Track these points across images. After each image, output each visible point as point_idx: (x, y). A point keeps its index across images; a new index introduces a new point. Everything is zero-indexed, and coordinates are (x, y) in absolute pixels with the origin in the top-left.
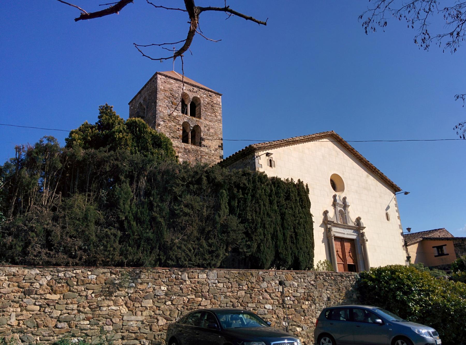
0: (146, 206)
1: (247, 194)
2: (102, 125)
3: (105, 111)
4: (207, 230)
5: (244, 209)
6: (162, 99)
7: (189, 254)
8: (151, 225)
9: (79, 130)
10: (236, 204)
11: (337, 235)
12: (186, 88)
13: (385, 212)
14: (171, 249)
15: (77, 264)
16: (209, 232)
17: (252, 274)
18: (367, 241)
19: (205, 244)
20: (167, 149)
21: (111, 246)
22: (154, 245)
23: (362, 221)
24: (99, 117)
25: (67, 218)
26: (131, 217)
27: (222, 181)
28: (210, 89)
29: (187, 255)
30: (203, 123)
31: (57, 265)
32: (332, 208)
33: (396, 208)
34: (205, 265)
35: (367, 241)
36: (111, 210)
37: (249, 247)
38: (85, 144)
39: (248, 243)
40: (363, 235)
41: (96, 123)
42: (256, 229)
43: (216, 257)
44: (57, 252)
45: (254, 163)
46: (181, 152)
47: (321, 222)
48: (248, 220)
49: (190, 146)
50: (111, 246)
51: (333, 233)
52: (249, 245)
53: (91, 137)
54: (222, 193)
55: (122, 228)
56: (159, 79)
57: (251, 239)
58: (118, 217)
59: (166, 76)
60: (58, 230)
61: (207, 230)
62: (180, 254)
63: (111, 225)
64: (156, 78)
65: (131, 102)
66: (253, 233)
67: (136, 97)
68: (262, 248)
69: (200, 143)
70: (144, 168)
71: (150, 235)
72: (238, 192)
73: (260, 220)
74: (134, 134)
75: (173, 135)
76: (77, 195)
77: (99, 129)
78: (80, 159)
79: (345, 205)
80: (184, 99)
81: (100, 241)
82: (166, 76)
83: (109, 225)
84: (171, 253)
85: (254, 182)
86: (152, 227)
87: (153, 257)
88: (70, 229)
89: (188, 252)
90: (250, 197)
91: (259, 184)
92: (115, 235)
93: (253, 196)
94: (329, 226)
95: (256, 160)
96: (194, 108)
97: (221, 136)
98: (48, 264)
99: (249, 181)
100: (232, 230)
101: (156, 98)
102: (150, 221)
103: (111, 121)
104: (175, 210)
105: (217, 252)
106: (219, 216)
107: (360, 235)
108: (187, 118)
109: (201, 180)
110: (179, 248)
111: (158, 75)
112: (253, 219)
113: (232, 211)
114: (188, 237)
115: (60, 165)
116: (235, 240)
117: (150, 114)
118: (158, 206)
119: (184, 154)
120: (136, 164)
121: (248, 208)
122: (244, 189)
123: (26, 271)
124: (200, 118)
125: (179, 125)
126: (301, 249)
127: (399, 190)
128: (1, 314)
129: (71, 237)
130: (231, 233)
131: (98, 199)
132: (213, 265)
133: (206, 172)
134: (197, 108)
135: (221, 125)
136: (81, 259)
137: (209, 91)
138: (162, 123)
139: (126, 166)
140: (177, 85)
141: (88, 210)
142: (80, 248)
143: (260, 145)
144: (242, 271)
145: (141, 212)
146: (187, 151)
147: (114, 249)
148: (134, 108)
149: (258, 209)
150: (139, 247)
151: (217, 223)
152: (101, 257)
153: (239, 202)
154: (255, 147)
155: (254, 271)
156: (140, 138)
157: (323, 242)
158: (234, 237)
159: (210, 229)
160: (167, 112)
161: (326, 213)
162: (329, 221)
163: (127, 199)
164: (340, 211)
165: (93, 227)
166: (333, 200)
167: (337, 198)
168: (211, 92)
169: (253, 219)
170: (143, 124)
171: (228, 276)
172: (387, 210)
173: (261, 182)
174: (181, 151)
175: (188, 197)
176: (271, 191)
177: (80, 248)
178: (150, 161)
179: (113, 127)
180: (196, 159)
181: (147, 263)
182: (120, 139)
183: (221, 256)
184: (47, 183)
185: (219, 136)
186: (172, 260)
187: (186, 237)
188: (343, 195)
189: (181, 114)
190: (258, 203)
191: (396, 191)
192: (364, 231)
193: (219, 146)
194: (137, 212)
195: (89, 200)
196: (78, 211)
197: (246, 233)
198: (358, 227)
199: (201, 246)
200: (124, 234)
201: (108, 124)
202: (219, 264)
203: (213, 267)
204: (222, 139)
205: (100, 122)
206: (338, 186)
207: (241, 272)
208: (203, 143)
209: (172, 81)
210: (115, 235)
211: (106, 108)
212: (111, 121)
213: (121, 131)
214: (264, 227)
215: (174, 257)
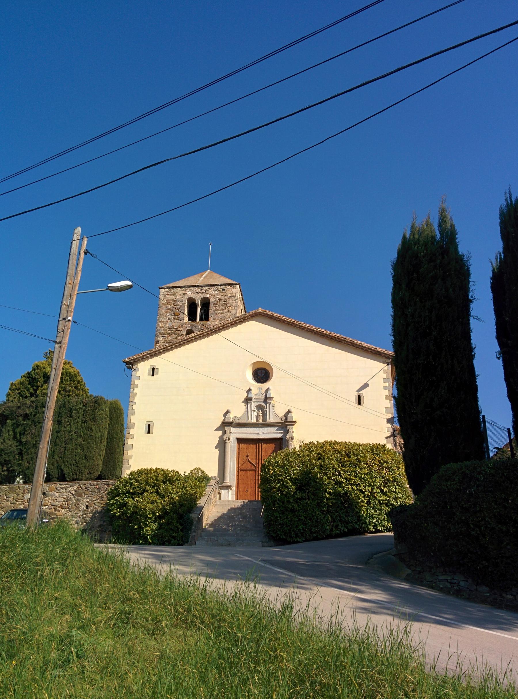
6: (163, 314)
12: (190, 293)
13: (356, 394)
59: (169, 288)
82: (169, 288)
128: (251, 698)
140: (181, 293)
203: (149, 503)
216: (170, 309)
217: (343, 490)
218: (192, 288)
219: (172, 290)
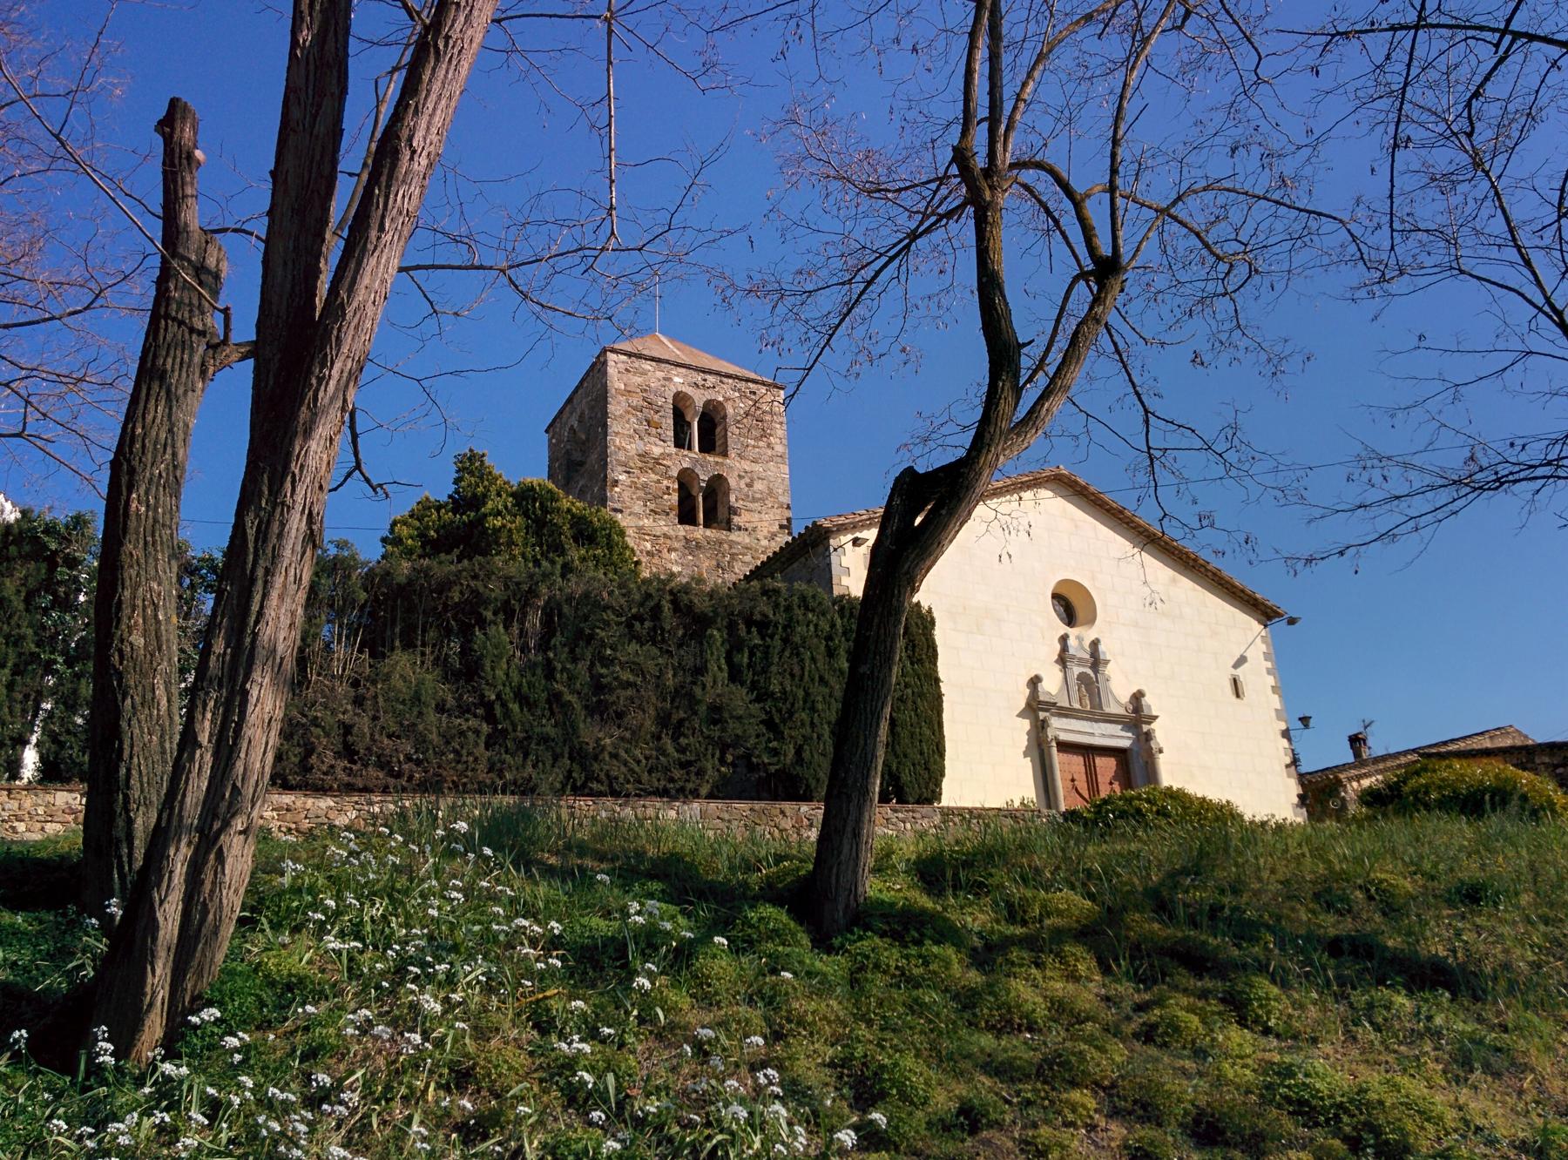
0: (539, 671)
1: (772, 637)
2: (463, 498)
3: (470, 465)
4: (675, 718)
5: (765, 671)
6: (621, 416)
7: (637, 769)
8: (551, 709)
9: (411, 516)
10: (746, 660)
11: (1063, 737)
12: (679, 380)
14: (596, 758)
15: (404, 790)
16: (681, 722)
17: (782, 812)
18: (1161, 751)
19: (670, 749)
20: (610, 546)
21: (469, 754)
22: (558, 750)
23: (1147, 700)
24: (457, 481)
25: (380, 699)
26: (508, 694)
27: (709, 611)
28: (753, 376)
29: (632, 771)
30: (734, 468)
31: (366, 790)
32: (1058, 667)
33: (1269, 665)
34: (673, 792)
35: (1161, 751)
36: (468, 682)
37: (775, 752)
38: (423, 546)
39: (774, 744)
40: (1148, 736)
41: (450, 497)
42: (791, 714)
43: (697, 774)
44: (366, 766)
45: (829, 565)
46: (675, 550)
47: (1022, 705)
48: (773, 693)
49: (699, 532)
50: (469, 754)
51: (1050, 733)
52: (775, 749)
53: (437, 531)
54: (712, 636)
55: (490, 718)
56: (611, 363)
57: (779, 736)
58: (482, 696)
59: (630, 355)
60: (364, 724)
61: (675, 718)
62: (618, 770)
63: (468, 711)
64: (605, 363)
65: (551, 425)
66: (784, 721)
67: (561, 412)
68: (806, 755)
69: (729, 521)
70: (533, 592)
71: (550, 730)
72: (749, 632)
73: (801, 693)
74: (528, 517)
75: (653, 506)
76: (398, 652)
77: (455, 512)
78: (402, 580)
79: (1096, 661)
80: (680, 405)
81: (448, 743)
82: (630, 355)
83: (464, 710)
84: (596, 766)
85: (788, 609)
86: (552, 714)
87: (556, 777)
88: (387, 720)
89: (634, 766)
90: (777, 642)
91: (798, 612)
92: (477, 732)
93: (785, 641)
94: (1042, 715)
95: (834, 557)
96: (710, 430)
97: (785, 499)
98: (349, 789)
99: (777, 606)
100: (732, 717)
101: (605, 414)
102: (548, 701)
103: (480, 489)
104: (602, 676)
105: (698, 765)
106: (704, 687)
107: (1143, 738)
108: (689, 458)
109: (676, 615)
110: (615, 756)
111: (611, 356)
112: (784, 692)
113: (735, 676)
114: (633, 733)
115: (363, 596)
116: (738, 741)
117: (594, 457)
118: (564, 669)
119: (684, 555)
120: (518, 584)
121: (774, 669)
122: (763, 626)
123: (310, 801)
124: (725, 454)
125: (669, 478)
126: (905, 756)
127: (1279, 615)
129: (389, 737)
130: (731, 724)
131: (441, 661)
132: (691, 792)
133: (671, 592)
134: (718, 430)
135: (786, 469)
136: (410, 778)
137: (748, 380)
138: (623, 477)
139: (495, 589)
140: (660, 374)
141: (421, 683)
142: (409, 758)
143: (842, 520)
144: (758, 805)
145: (529, 683)
146: (691, 546)
147: (476, 759)
148: (559, 442)
149: (797, 670)
150: (526, 755)
151: (699, 702)
152: (450, 775)
153: (752, 654)
154: (827, 524)
155: (788, 806)
156: (545, 524)
157: (1026, 755)
158: (739, 732)
159: (682, 714)
160: (634, 447)
161: (1035, 682)
162: (1040, 702)
163: (500, 657)
164: (1082, 678)
165: (432, 716)
166: (1058, 647)
167: (1072, 642)
168: (754, 381)
169: (784, 692)
170: (550, 491)
171: (726, 816)
172: (1237, 665)
173: (807, 608)
174: (676, 545)
175: (633, 647)
176: (833, 626)
177: (409, 758)
178: (545, 576)
179: (484, 504)
180: (718, 566)
181: (544, 787)
182: (497, 531)
183: (710, 772)
184: (340, 635)
185: (781, 499)
186: (599, 781)
187: (628, 735)
188: (1089, 634)
189: (673, 450)
190: (798, 655)
191: (1270, 618)
192: (1153, 726)
193: (781, 527)
194: (520, 685)
195: (423, 663)
196: (400, 684)
197: (769, 724)
198: (1137, 717)
199: (664, 753)
200: (495, 729)
201: (475, 495)
202: (704, 791)
204: (788, 507)
205: (457, 492)
206: (1080, 613)
207: (757, 807)
208: (736, 519)
209: (647, 366)
210: (477, 732)
211: (470, 459)
212: (480, 489)
213: (499, 513)
214: (813, 709)
215: (602, 776)
216: (635, 408)
217: (1240, 1045)
218: (683, 370)
219: (637, 363)
